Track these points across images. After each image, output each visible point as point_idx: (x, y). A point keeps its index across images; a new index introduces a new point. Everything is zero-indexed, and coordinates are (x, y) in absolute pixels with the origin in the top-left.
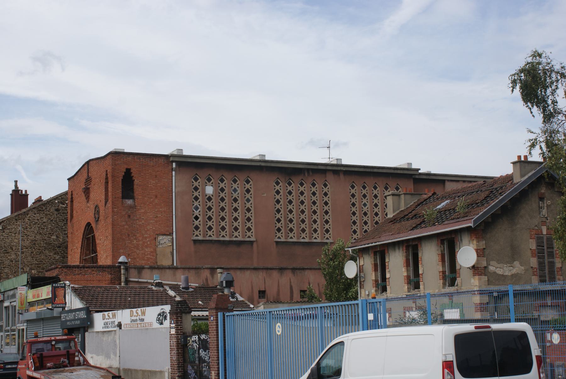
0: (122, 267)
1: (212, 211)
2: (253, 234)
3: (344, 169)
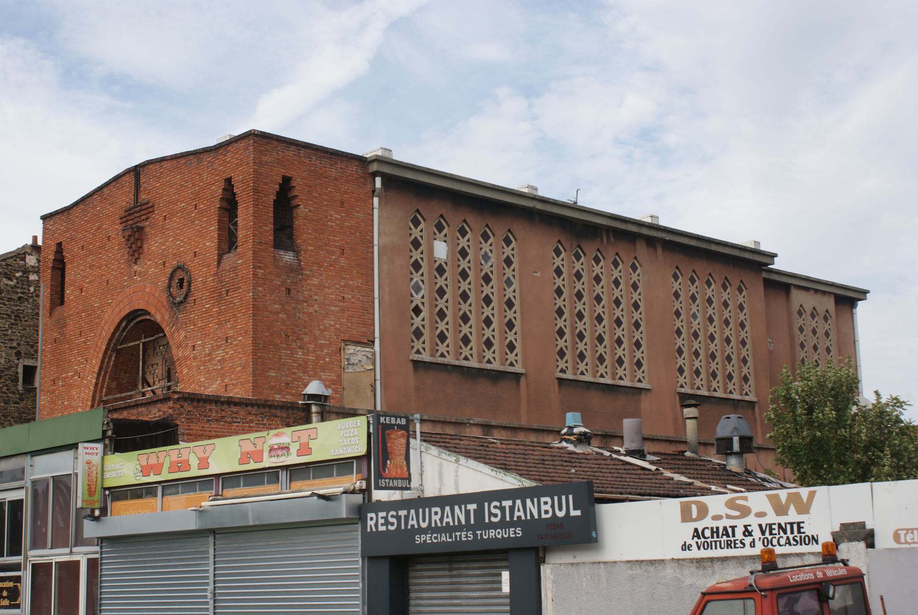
0: (314, 409)
1: (446, 297)
2: (519, 358)
3: (668, 237)
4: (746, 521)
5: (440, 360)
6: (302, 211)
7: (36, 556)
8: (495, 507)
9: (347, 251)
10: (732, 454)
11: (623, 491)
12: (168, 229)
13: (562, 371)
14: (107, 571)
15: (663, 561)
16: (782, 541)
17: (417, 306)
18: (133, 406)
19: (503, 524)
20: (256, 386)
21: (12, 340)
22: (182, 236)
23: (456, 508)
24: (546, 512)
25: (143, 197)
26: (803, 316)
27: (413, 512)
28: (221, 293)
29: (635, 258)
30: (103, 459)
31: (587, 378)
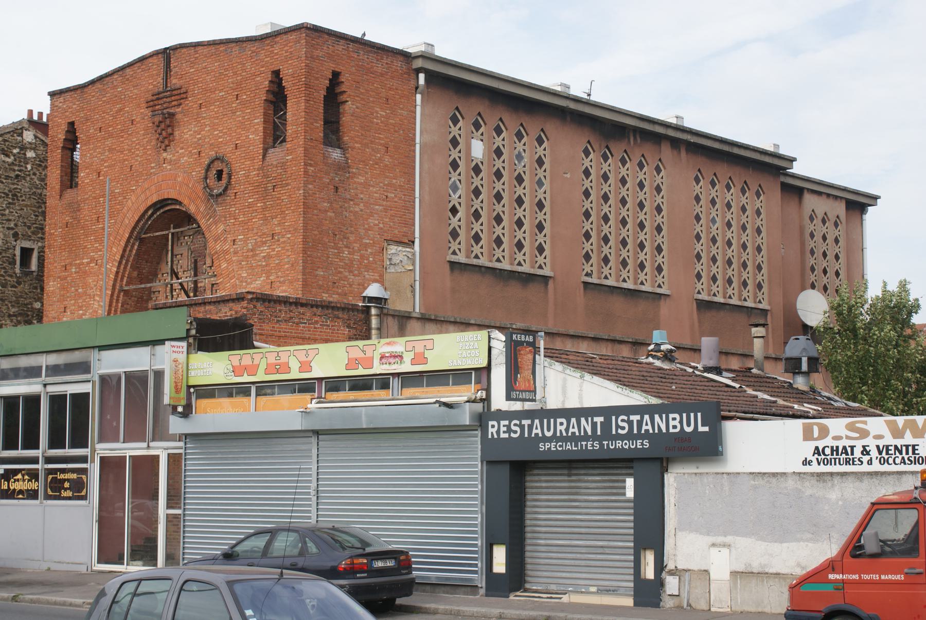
2: (548, 261)
3: (693, 139)
4: (864, 442)
5: (475, 262)
6: (349, 108)
7: (106, 449)
8: (623, 421)
9: (391, 149)
10: (800, 373)
11: (731, 408)
12: (204, 118)
13: (587, 275)
14: (193, 466)
15: (785, 473)
16: (898, 461)
17: (454, 206)
18: (200, 304)
19: (630, 436)
20: (305, 284)
21: (9, 220)
22: (225, 125)
23: (583, 420)
24: (674, 427)
25: (174, 82)
26: (815, 222)
27: (537, 421)
28: (268, 187)
29: (660, 160)
30: (188, 358)
31: (611, 282)
